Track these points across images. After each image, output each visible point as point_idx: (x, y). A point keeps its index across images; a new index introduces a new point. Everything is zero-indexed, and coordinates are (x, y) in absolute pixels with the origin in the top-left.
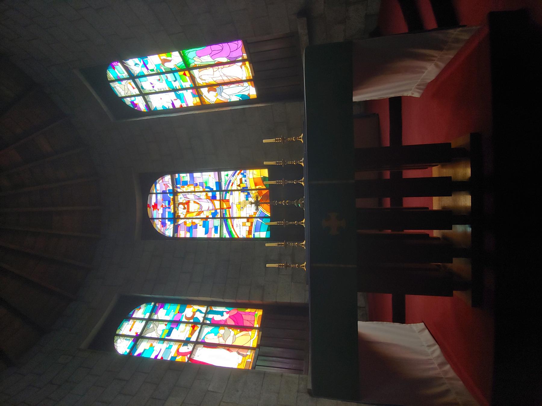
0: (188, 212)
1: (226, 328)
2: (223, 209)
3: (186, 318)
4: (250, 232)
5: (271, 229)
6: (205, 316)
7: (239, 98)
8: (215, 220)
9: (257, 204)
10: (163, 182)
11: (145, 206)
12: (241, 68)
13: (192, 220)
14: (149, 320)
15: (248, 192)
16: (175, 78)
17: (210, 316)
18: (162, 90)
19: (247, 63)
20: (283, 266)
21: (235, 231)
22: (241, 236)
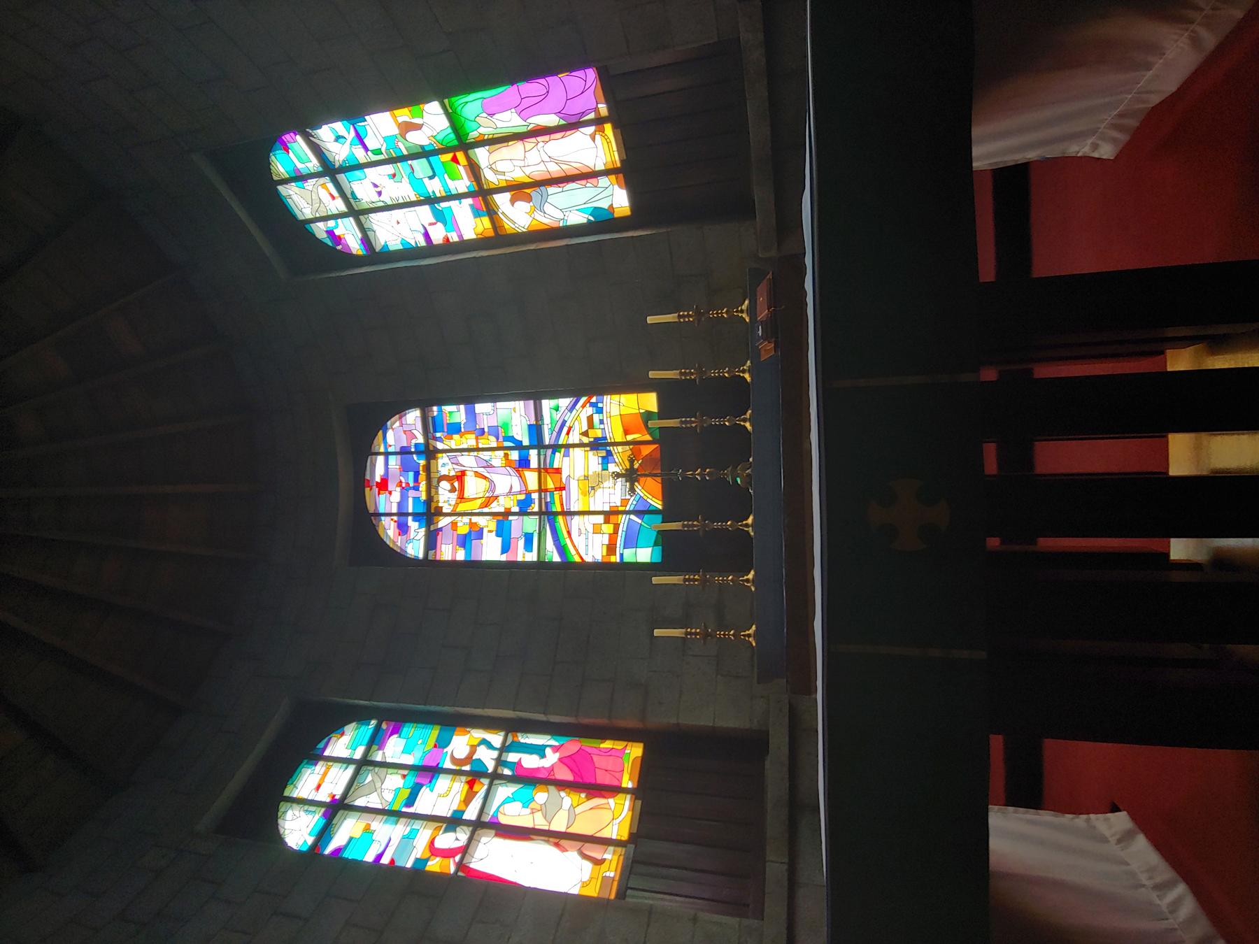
0: (461, 498)
1: (552, 788)
2: (546, 490)
3: (453, 758)
4: (611, 548)
5: (665, 540)
6: (500, 755)
7: (587, 216)
8: (526, 518)
9: (631, 476)
10: (402, 425)
11: (360, 482)
12: (594, 139)
13: (470, 517)
14: (365, 763)
15: (608, 448)
16: (434, 172)
17: (512, 757)
18: (401, 201)
19: (608, 128)
20: (696, 634)
21: (574, 546)
22: (588, 559)
